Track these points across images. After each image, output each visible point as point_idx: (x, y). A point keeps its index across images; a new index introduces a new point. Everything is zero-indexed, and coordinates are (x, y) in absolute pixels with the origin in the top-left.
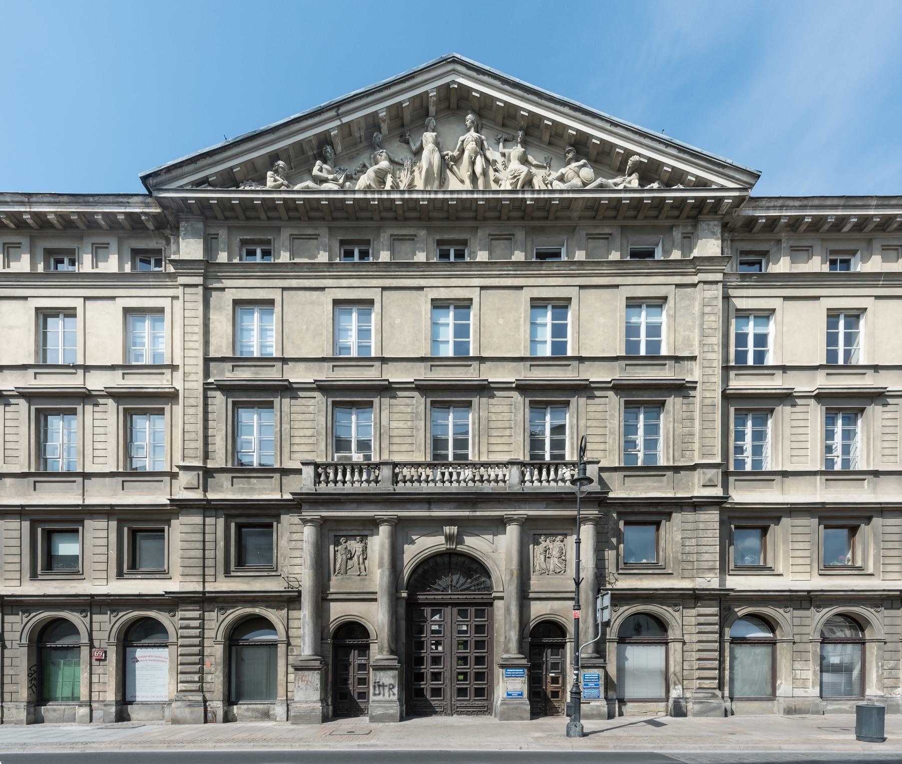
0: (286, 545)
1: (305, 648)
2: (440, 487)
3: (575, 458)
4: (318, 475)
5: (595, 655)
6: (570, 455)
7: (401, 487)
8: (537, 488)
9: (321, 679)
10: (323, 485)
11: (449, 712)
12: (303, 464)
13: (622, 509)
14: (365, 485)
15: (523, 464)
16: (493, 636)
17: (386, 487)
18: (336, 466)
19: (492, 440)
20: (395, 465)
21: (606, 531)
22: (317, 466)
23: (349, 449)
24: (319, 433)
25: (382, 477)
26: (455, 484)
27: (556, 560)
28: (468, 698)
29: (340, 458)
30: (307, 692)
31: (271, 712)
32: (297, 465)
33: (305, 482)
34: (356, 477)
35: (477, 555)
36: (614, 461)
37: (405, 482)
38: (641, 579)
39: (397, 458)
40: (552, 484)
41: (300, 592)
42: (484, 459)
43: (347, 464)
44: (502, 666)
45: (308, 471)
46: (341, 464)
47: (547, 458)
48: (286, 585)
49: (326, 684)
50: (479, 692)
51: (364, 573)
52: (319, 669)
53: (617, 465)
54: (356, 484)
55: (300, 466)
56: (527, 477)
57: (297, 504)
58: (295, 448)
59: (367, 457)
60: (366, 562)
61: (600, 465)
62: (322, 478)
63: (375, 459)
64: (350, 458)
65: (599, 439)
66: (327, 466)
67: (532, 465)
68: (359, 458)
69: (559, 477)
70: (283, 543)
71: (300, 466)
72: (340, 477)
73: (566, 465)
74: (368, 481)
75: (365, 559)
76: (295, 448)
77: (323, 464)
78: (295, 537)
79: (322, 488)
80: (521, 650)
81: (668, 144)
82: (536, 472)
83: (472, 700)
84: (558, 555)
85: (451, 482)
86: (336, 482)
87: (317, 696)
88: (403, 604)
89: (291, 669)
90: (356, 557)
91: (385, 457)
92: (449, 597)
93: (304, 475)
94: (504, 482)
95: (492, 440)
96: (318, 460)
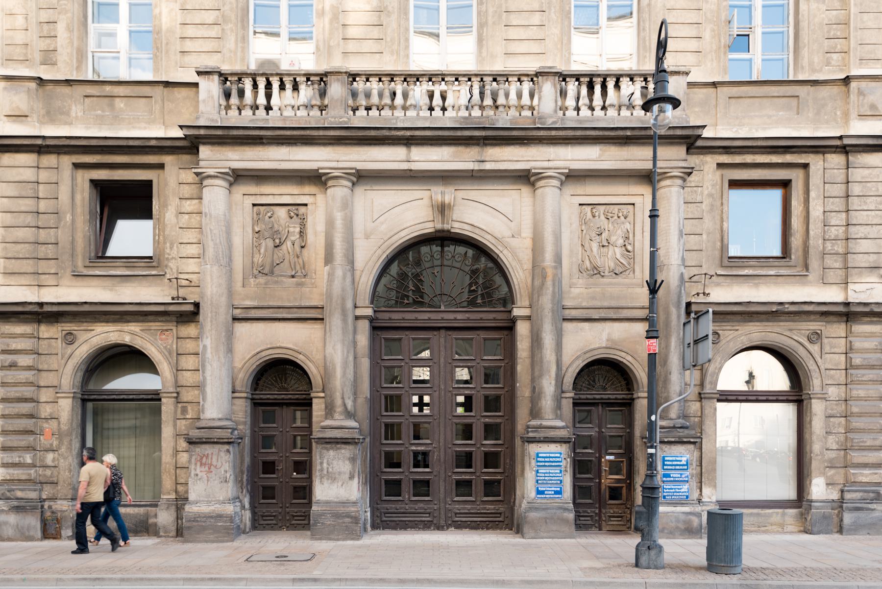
12: (199, 73)
18: (254, 77)
20: (353, 77)
22: (224, 77)
24: (225, 19)
42: (498, 67)
46: (262, 75)
61: (691, 78)
66: (240, 77)
84: (620, 242)
96: (226, 68)
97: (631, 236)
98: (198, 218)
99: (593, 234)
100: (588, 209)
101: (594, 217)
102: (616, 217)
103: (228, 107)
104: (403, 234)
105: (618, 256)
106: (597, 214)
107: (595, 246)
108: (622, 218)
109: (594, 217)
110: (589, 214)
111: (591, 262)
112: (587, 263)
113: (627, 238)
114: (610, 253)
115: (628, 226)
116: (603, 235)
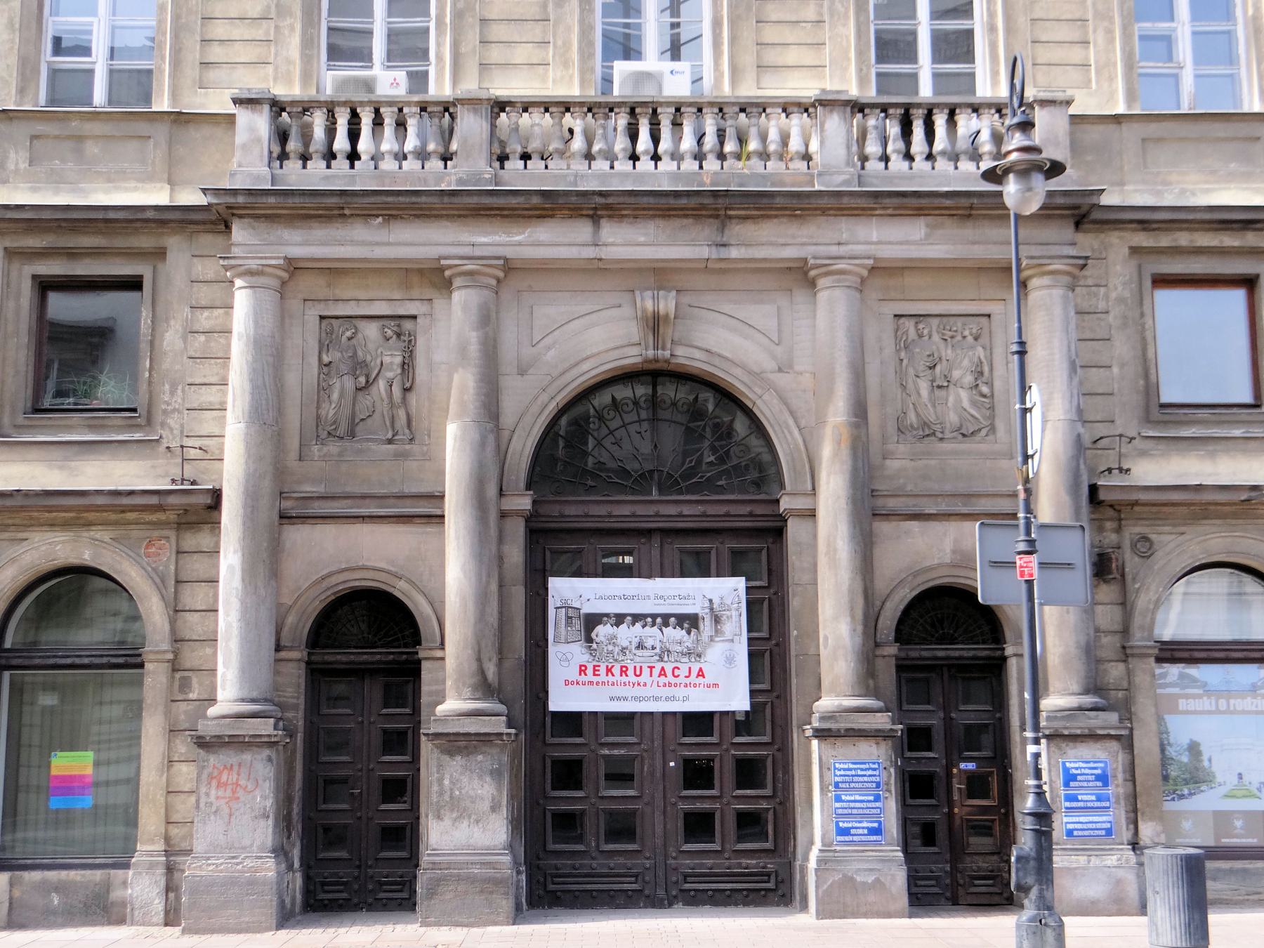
0: (179, 344)
1: (232, 669)
2: (625, 175)
3: (1003, 92)
4: (282, 136)
5: (1089, 700)
6: (990, 83)
7: (517, 176)
8: (901, 177)
9: (277, 780)
10: (293, 165)
11: (661, 893)
12: (237, 101)
13: (1143, 239)
14: (411, 165)
15: (859, 107)
16: (785, 635)
17: (470, 168)
19: (770, 34)
21: (1102, 306)
22: (278, 107)
23: (364, 56)
25: (464, 142)
26: (666, 165)
27: (964, 395)
28: (713, 739)
29: (343, 84)
30: (236, 825)
31: (116, 894)
32: (218, 103)
33: (246, 159)
34: (388, 143)
35: (736, 380)
36: (1112, 96)
37: (526, 157)
38: (1212, 455)
39: (501, 89)
40: (942, 164)
41: (217, 495)
42: (748, 90)
43: (362, 104)
44: (821, 734)
45: (257, 125)
47: (926, 91)
48: (176, 472)
49: (289, 799)
50: (749, 823)
51: (404, 435)
52: (272, 744)
53: (1121, 109)
54: (390, 160)
55: (231, 109)
56: (873, 148)
57: (216, 218)
58: (216, 54)
59: (419, 80)
60: (413, 398)
61: (1073, 110)
62: (293, 145)
63: (440, 87)
64: (369, 85)
65: (1065, 33)
66: (306, 108)
67: (884, 108)
68: (395, 84)
69: (963, 144)
70: (171, 338)
71: (231, 109)
72: (341, 143)
73: (976, 109)
74: (422, 155)
75: (407, 390)
76: (216, 54)
77: (293, 103)
78: (205, 320)
79: (296, 176)
80: (867, 679)
81: (856, 209)
82: (894, 129)
83: (724, 853)
84: (969, 379)
85: (656, 158)
86: (330, 156)
87: (264, 833)
88: (517, 529)
89: (183, 747)
90: (382, 384)
91: (470, 86)
92: (651, 510)
93: (241, 136)
94: (807, 157)
95: (770, 34)
96: (281, 91)
97: (986, 369)
99: (922, 365)
100: (909, 325)
101: (921, 336)
102: (959, 338)
105: (966, 404)
106: (926, 332)
108: (970, 339)
109: (921, 336)
111: (918, 415)
113: (981, 373)
114: (951, 399)
115: (980, 352)
116: (938, 368)
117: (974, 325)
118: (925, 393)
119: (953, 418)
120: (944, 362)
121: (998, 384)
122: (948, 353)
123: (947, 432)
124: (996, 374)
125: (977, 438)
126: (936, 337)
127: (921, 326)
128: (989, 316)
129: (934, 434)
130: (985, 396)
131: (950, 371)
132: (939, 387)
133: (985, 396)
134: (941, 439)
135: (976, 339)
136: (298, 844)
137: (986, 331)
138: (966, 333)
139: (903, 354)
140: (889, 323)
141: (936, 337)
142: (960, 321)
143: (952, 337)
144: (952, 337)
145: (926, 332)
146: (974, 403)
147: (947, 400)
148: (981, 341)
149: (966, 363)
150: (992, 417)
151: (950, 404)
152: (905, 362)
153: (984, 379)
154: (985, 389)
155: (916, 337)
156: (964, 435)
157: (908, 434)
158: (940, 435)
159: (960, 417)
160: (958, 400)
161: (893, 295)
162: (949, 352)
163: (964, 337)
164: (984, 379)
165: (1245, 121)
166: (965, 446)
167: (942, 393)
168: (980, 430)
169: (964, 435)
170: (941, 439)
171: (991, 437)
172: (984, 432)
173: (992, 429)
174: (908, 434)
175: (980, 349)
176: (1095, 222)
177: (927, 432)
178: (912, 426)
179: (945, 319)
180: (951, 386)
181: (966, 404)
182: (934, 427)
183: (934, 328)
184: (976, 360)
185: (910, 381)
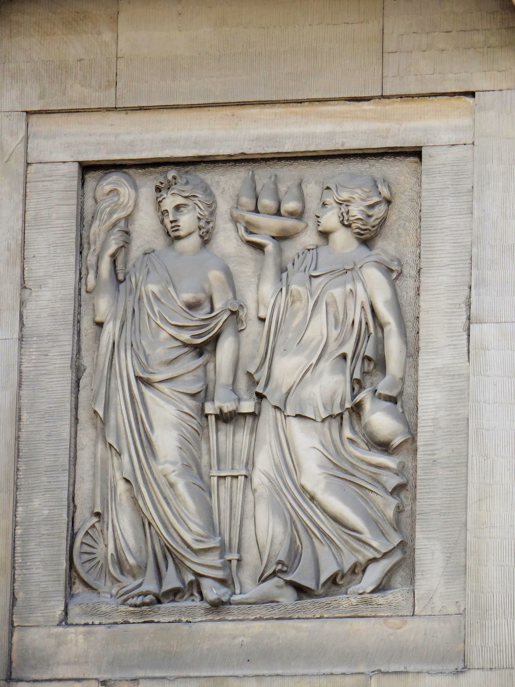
27: (308, 444)
84: (329, 385)
97: (394, 347)
98: (464, 454)
99: (161, 343)
100: (136, 199)
101: (173, 237)
102: (309, 238)
103: (164, 198)
104: (278, 453)
105: (313, 475)
106: (187, 221)
107: (167, 417)
108: (343, 240)
109: (173, 237)
110: (146, 228)
111: (144, 524)
112: (124, 526)
113: (379, 363)
114: (264, 462)
115: (376, 286)
116: (226, 348)
117: (354, 190)
118: (167, 441)
119: (266, 530)
120: (252, 330)
121: (431, 401)
122: (260, 293)
123: (247, 577)
124: (426, 362)
125: (345, 600)
126: (227, 240)
127: (170, 202)
128: (416, 153)
129: (195, 587)
130: (384, 447)
131: (268, 358)
132: (224, 418)
133: (384, 447)
134: (217, 606)
135: (366, 240)
136: (183, 335)
137: (402, 207)
138: (330, 219)
139: (104, 305)
140: (56, 196)
141: (227, 240)
142: (314, 175)
143: (282, 237)
144: (282, 237)
145: (187, 221)
146: (342, 472)
147: (250, 463)
148: (386, 247)
149: (319, 328)
150: (403, 522)
151: (258, 479)
152: (110, 330)
153: (383, 386)
154: (381, 421)
155: (159, 242)
156: (301, 591)
157: (106, 587)
158: (212, 591)
159: (292, 524)
160: (289, 464)
161: (76, 94)
162: (268, 289)
163: (325, 235)
164: (383, 386)
165: (296, 164)
166: (305, 629)
167: (233, 440)
168: (358, 570)
169: (301, 591)
170: (217, 606)
171: (396, 596)
172: (373, 575)
173: (403, 560)
174: (106, 587)
175: (374, 276)
176: (236, 226)
177: (171, 581)
178: (120, 562)
179: (263, 175)
180: (268, 414)
181: (313, 475)
182: (196, 563)
183: (224, 207)
184: (356, 314)
185: (120, 401)
